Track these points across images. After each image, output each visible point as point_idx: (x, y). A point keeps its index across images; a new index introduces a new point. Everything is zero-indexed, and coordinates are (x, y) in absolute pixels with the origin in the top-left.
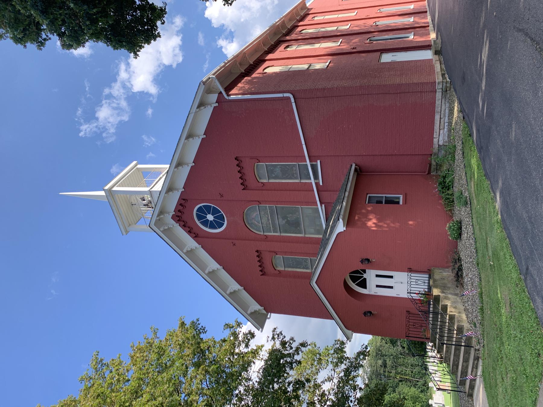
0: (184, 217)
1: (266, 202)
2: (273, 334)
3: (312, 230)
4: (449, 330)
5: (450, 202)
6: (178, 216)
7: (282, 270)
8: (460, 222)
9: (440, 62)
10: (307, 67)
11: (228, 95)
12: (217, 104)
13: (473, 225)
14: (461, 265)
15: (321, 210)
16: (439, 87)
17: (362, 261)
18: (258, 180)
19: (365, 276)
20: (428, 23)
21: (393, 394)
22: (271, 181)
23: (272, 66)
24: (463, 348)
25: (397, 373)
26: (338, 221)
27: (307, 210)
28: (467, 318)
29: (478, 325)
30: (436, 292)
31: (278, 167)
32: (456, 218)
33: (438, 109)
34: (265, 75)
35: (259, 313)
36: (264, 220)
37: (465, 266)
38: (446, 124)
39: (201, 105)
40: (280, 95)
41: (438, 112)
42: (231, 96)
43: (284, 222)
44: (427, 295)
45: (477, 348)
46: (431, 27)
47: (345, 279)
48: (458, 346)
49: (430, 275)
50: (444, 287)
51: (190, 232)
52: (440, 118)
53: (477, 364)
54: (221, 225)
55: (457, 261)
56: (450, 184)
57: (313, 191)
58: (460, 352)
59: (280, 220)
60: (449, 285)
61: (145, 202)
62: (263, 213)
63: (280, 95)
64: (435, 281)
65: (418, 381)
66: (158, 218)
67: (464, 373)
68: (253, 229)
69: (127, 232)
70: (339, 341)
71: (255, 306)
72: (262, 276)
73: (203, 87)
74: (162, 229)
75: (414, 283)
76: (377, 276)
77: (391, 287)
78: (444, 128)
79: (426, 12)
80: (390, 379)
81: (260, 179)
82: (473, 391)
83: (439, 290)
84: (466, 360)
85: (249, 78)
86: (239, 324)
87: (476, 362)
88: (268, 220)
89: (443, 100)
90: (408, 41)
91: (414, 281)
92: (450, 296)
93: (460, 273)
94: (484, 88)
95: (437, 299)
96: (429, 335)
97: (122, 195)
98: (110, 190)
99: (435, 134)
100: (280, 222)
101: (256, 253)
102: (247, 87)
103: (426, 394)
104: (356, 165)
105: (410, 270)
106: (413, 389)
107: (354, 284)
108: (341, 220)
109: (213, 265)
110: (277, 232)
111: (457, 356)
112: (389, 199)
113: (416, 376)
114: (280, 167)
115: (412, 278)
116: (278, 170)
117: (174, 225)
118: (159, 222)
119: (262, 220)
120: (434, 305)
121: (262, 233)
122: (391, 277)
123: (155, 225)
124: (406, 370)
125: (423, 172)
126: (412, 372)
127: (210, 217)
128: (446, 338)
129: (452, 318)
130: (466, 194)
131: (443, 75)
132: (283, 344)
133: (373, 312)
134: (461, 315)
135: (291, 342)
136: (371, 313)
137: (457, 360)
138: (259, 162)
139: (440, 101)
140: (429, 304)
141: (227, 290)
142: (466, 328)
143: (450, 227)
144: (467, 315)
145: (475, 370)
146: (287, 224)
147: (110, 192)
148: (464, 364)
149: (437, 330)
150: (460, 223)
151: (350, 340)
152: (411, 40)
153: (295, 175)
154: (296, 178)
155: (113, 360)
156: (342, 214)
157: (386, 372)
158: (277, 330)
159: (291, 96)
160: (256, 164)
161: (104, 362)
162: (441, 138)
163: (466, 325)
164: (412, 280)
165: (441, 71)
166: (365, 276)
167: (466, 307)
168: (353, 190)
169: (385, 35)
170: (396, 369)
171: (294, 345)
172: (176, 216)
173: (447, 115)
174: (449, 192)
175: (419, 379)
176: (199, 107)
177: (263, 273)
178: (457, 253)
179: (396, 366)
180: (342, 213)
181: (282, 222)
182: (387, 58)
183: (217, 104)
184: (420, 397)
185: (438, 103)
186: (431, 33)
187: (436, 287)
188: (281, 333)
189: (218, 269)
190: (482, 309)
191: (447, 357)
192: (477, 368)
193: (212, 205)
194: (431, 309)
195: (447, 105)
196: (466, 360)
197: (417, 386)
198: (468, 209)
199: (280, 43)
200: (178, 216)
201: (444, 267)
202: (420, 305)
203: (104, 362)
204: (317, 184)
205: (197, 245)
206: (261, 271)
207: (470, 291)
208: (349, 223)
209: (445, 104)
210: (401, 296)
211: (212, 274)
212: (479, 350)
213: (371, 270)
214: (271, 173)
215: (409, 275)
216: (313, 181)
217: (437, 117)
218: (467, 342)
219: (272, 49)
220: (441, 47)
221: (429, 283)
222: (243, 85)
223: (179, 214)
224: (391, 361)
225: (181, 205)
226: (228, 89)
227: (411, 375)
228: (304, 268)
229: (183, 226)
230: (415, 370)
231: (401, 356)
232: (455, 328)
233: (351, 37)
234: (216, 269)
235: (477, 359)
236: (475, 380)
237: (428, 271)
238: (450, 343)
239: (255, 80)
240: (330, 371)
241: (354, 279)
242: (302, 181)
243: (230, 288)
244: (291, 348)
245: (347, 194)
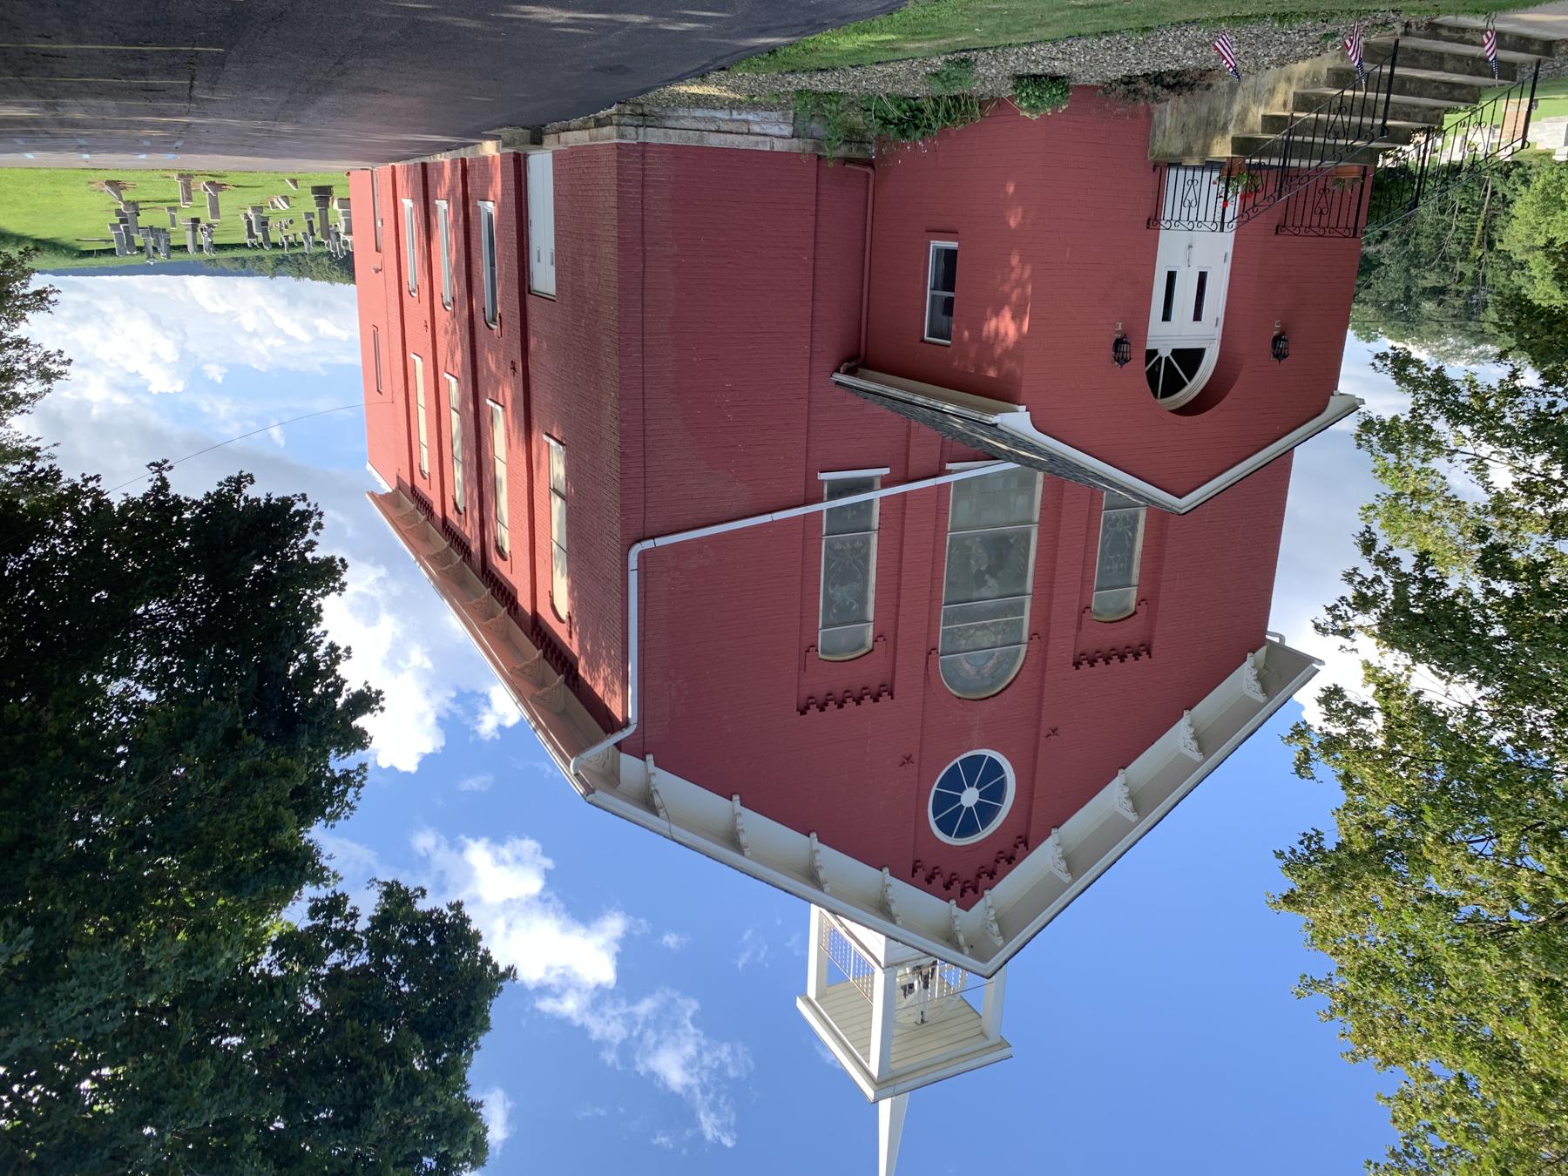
0: (969, 875)
1: (931, 632)
2: (1334, 632)
3: (1021, 500)
4: (1340, 110)
5: (957, 105)
6: (963, 891)
8: (1019, 80)
9: (564, 131)
10: (559, 500)
11: (626, 724)
12: (650, 757)
13: (1031, 45)
15: (960, 473)
16: (633, 136)
17: (1122, 360)
18: (865, 651)
19: (1165, 352)
20: (454, 162)
21: (1531, 270)
22: (871, 616)
23: (552, 597)
24: (1398, 71)
25: (1465, 256)
26: (1000, 426)
27: (958, 512)
28: (1305, 57)
29: (1330, 28)
30: (1222, 149)
31: (831, 591)
32: (1007, 90)
33: (692, 139)
34: (574, 620)
35: (1265, 667)
36: (986, 639)
37: (1148, 66)
38: (735, 115)
39: (647, 801)
40: (633, 578)
41: (702, 137)
42: (630, 716)
43: (992, 582)
44: (1229, 174)
45: (1399, 29)
46: (466, 153)
47: (1172, 411)
48: (1391, 84)
49: (1170, 165)
50: (1208, 124)
51: (1012, 861)
52: (718, 131)
53: (1450, 29)
54: (995, 768)
55: (1132, 87)
56: (904, 106)
57: (904, 494)
58: (1411, 79)
59: (985, 592)
60: (1204, 110)
61: (916, 983)
62: (963, 642)
63: (633, 578)
64: (1188, 151)
65: (1494, 193)
66: (967, 951)
67: (1477, 66)
68: (1009, 670)
69: (1003, 1044)
70: (1360, 436)
71: (1244, 679)
72: (1153, 654)
73: (601, 796)
74: (1000, 942)
75: (1193, 211)
76: (1166, 317)
77: (1202, 277)
78: (746, 121)
79: (424, 165)
80: (1484, 277)
81: (862, 645)
82: (1535, 39)
83: (1217, 139)
84: (1438, 60)
85: (582, 663)
86: (1297, 733)
87: (1445, 33)
88: (984, 627)
89: (669, 123)
90: (499, 217)
91: (1185, 210)
92: (1236, 108)
93: (1169, 80)
94: (646, 18)
95: (1244, 146)
96: (1352, 168)
97: (893, 1050)
98: (877, 1084)
99: (761, 147)
102: (605, 671)
103: (1533, 170)
104: (838, 371)
105: (1154, 222)
106: (1518, 209)
107: (1190, 385)
108: (994, 419)
109: (1112, 798)
110: (1022, 605)
111: (1422, 87)
112: (941, 279)
113: (1476, 198)
114: (833, 585)
115: (1176, 217)
116: (839, 593)
117: (989, 903)
118: (979, 949)
119: (984, 645)
120: (1261, 155)
121: (1024, 648)
122: (1171, 276)
123: (984, 959)
124: (1458, 228)
125: (868, 182)
126: (1462, 211)
127: (970, 797)
128: (1367, 120)
129: (1303, 102)
130: (938, 62)
131: (600, 123)
132: (1363, 603)
133: (1275, 333)
134: (1296, 76)
135: (1358, 579)
136: (1277, 339)
137: (1436, 87)
138: (814, 646)
139: (671, 132)
140: (1260, 166)
142: (1338, 61)
143: (1032, 108)
144: (1298, 59)
145: (1468, 36)
146: (1000, 574)
147: (884, 1084)
148: (1448, 66)
149: (1340, 146)
150: (1020, 78)
151: (1357, 402)
152: (499, 207)
153: (858, 544)
154: (867, 542)
156: (978, 415)
157: (1461, 289)
158: (1321, 621)
159: (638, 548)
160: (821, 656)
161: (1400, 1148)
162: (775, 130)
163: (1328, 61)
164: (1184, 217)
165: (588, 129)
166: (1165, 352)
167: (1271, 62)
169: (481, 280)
170: (1453, 260)
171: (1368, 571)
172: (962, 895)
173: (712, 113)
174: (928, 112)
175: (1486, 190)
176: (652, 808)
177: (1143, 649)
178: (1108, 87)
179: (1443, 259)
180: (976, 415)
181: (992, 586)
182: (544, 277)
183: (650, 757)
184: (1544, 189)
185: (675, 138)
186: (483, 154)
187: (1207, 148)
188: (1330, 610)
189: (1125, 785)
190: (1282, 18)
191: (1425, 116)
192: (1464, 30)
193: (935, 788)
194: (1275, 162)
195: (681, 112)
196: (1438, 60)
197: (1509, 197)
198: (983, 56)
199: (490, 571)
200: (963, 891)
201: (1147, 124)
202: (1260, 196)
203: (1400, 1148)
204: (886, 482)
206: (1137, 656)
207: (1227, 49)
208: (1005, 395)
209: (678, 118)
210: (1229, 248)
211: (1140, 802)
212: (1408, 25)
214: (848, 615)
215: (1168, 225)
216: (876, 495)
217: (715, 141)
218: (1380, 59)
219: (504, 593)
220: (524, 128)
221: (1194, 168)
222: (601, 682)
223: (957, 886)
224: (1427, 275)
225: (929, 880)
226: (609, 724)
227: (1473, 213)
228: (1134, 529)
229: (991, 878)
230: (1458, 202)
231: (1412, 241)
232: (1335, 92)
233: (483, 373)
234: (1127, 790)
235: (1433, 30)
236: (1500, 36)
237: (1158, 169)
238: (1381, 109)
239: (588, 647)
240: (1453, 464)
241: (1174, 385)
242: (876, 527)
243: (1186, 752)
244: (1377, 580)
245: (920, 399)
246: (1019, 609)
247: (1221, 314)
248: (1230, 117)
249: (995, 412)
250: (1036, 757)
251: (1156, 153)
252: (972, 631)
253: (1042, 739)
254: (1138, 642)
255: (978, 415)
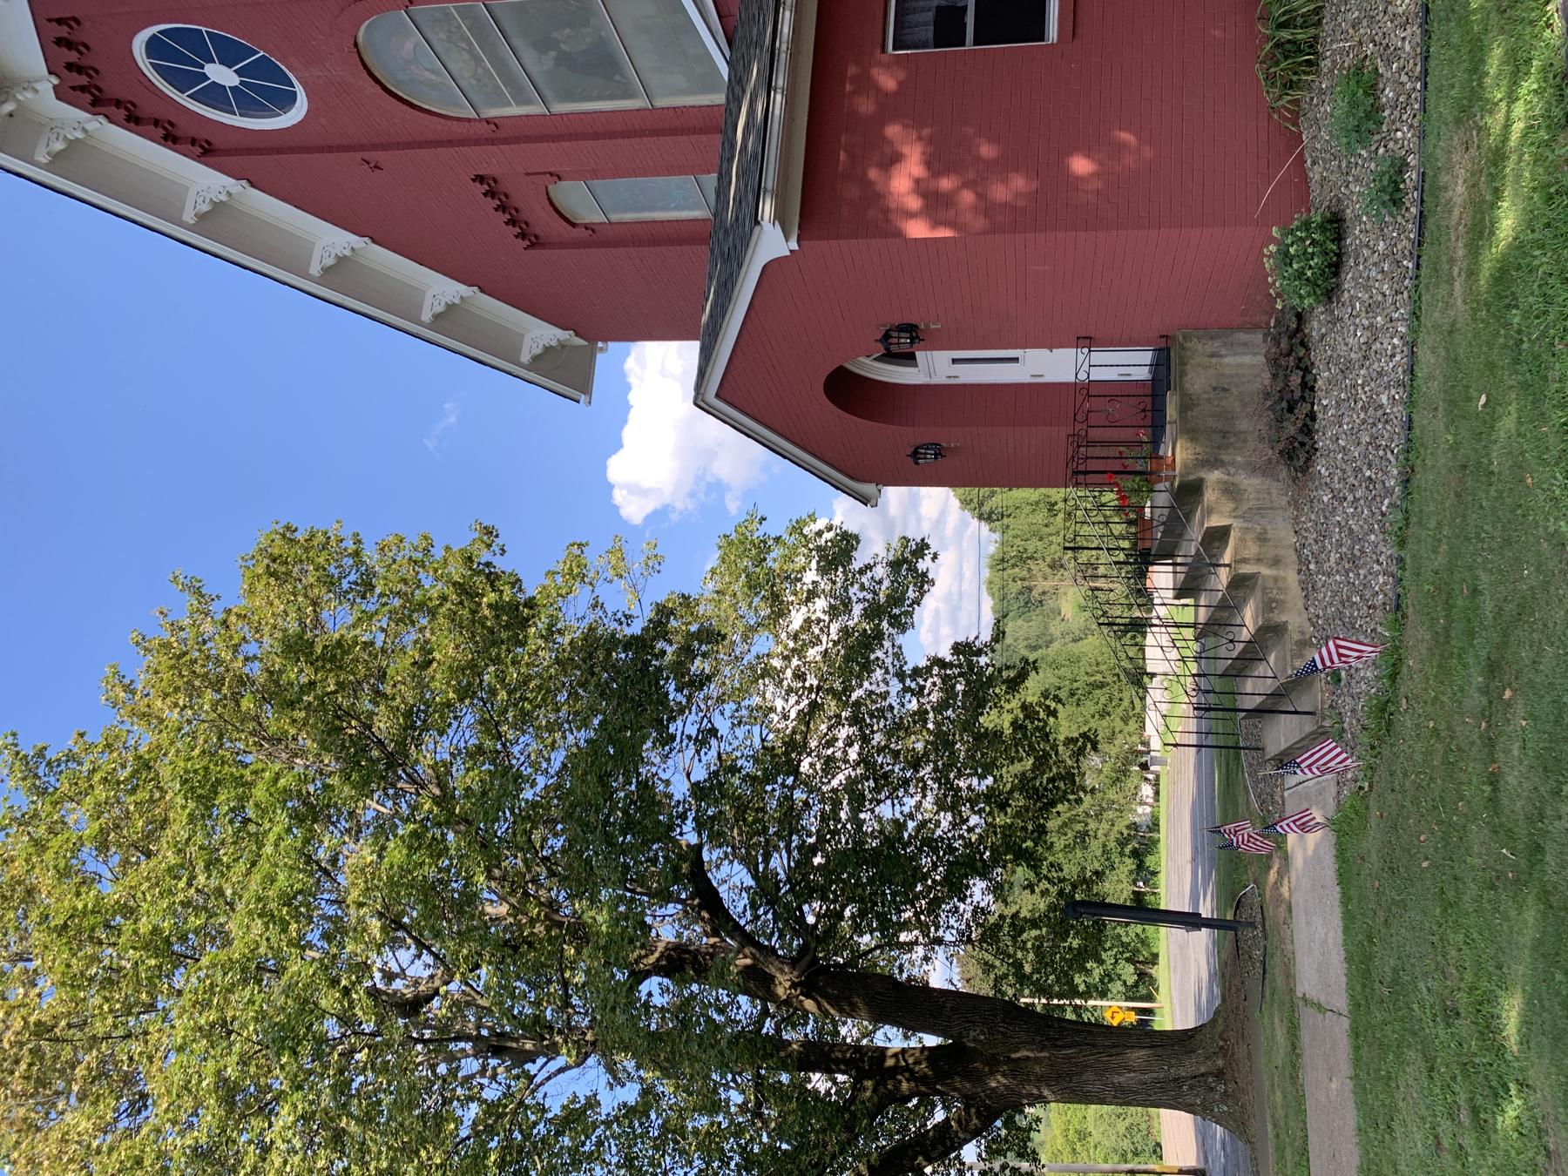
0: (112, 85)
7: (600, 224)
8: (1336, 225)
14: (1312, 416)
26: (757, 229)
51: (171, 139)
59: (529, 56)
71: (539, 334)
72: (532, 252)
74: (43, 158)
76: (955, 361)
88: (478, 61)
100: (529, 66)
101: (478, 184)
108: (767, 209)
117: (89, 127)
122: (1016, 360)
141: (420, 308)
143: (1285, 258)
151: (873, 502)
155: (82, 735)
156: (770, 186)
168: (807, 109)
180: (770, 181)
189: (353, 249)
205: (229, 181)
211: (340, 273)
213: (935, 353)
246: (522, 100)
247: (961, 381)
248: (1232, 470)
249: (781, 217)
250: (330, 149)
251: (1186, 345)
252: (464, 45)
253: (359, 155)
254: (538, 231)
255: (780, 83)
